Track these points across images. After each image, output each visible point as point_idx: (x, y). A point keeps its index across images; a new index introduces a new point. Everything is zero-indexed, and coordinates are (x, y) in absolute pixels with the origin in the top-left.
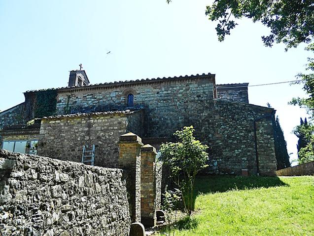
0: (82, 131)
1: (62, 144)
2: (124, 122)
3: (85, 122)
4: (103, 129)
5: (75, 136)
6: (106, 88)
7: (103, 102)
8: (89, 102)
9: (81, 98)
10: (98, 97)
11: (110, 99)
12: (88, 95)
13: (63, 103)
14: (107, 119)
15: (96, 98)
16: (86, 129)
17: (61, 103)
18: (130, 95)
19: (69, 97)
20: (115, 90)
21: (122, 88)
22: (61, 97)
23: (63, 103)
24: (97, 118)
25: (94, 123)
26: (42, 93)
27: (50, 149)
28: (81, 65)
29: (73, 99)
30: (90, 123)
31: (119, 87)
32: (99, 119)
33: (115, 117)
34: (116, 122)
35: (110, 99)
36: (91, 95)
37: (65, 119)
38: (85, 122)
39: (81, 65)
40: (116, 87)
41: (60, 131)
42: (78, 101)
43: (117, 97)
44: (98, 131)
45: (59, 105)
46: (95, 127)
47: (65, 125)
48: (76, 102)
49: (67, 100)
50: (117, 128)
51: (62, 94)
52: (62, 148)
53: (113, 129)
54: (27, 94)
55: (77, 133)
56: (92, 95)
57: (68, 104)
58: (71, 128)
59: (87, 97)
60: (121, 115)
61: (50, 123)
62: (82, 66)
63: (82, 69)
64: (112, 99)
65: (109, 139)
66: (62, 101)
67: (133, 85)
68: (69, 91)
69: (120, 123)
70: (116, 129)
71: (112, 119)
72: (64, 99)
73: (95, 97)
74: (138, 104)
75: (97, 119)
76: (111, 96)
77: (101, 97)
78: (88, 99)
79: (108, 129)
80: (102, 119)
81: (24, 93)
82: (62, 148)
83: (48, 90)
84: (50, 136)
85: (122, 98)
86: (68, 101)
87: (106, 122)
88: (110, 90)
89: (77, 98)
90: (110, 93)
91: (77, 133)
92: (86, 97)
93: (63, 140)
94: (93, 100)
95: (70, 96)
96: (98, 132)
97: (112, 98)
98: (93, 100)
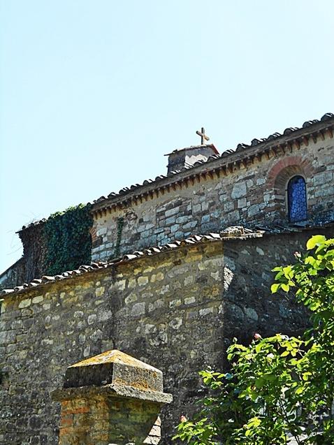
0: (96, 325)
1: (44, 375)
2: (216, 276)
3: (102, 289)
4: (151, 308)
5: (78, 341)
6: (217, 171)
7: (212, 220)
8: (174, 228)
9: (150, 222)
10: (197, 209)
11: (232, 206)
12: (170, 207)
13: (108, 246)
14: (164, 271)
15: (190, 213)
16: (106, 316)
17: (102, 247)
18: (292, 181)
19: (121, 223)
20: (243, 172)
21: (265, 160)
22: (102, 227)
23: (108, 246)
24: (137, 271)
25: (128, 291)
26: (56, 221)
27: (18, 391)
28: (201, 134)
29: (131, 228)
30: (116, 292)
31: (256, 162)
32: (141, 274)
33: (188, 260)
34: (189, 280)
35: (232, 206)
36: (176, 205)
37: (55, 287)
38: (102, 289)
39: (201, 134)
40: (247, 162)
41: (42, 331)
42: (145, 230)
43: (253, 197)
44: (137, 319)
45: (98, 253)
46: (131, 304)
47: (53, 307)
48: (139, 234)
49: (116, 235)
50: (192, 300)
51: (104, 218)
52: (44, 386)
53: (183, 307)
54: (28, 234)
55: (82, 331)
56: (179, 204)
57: (118, 246)
58: (66, 316)
59: (168, 213)
60: (207, 250)
61: (21, 306)
62: (206, 134)
63: (206, 143)
64: (236, 208)
65: (170, 345)
66: (105, 239)
67: (299, 142)
68: (120, 206)
69: (202, 280)
70: (192, 306)
71: (180, 270)
72: (109, 233)
73: (189, 208)
74: (321, 207)
75: (137, 277)
76: (234, 195)
77: (205, 207)
78: (169, 221)
79: (166, 310)
80: (149, 275)
81: (19, 232)
82: (44, 386)
83: (55, 219)
84: (19, 348)
85: (267, 198)
86: (120, 235)
87: (160, 284)
88: (229, 178)
89: (141, 221)
90: (230, 187)
91: (82, 331)
92: (162, 213)
93: (47, 361)
94: (182, 219)
95: (122, 219)
96: (137, 324)
97: (236, 204)
98: (182, 219)
